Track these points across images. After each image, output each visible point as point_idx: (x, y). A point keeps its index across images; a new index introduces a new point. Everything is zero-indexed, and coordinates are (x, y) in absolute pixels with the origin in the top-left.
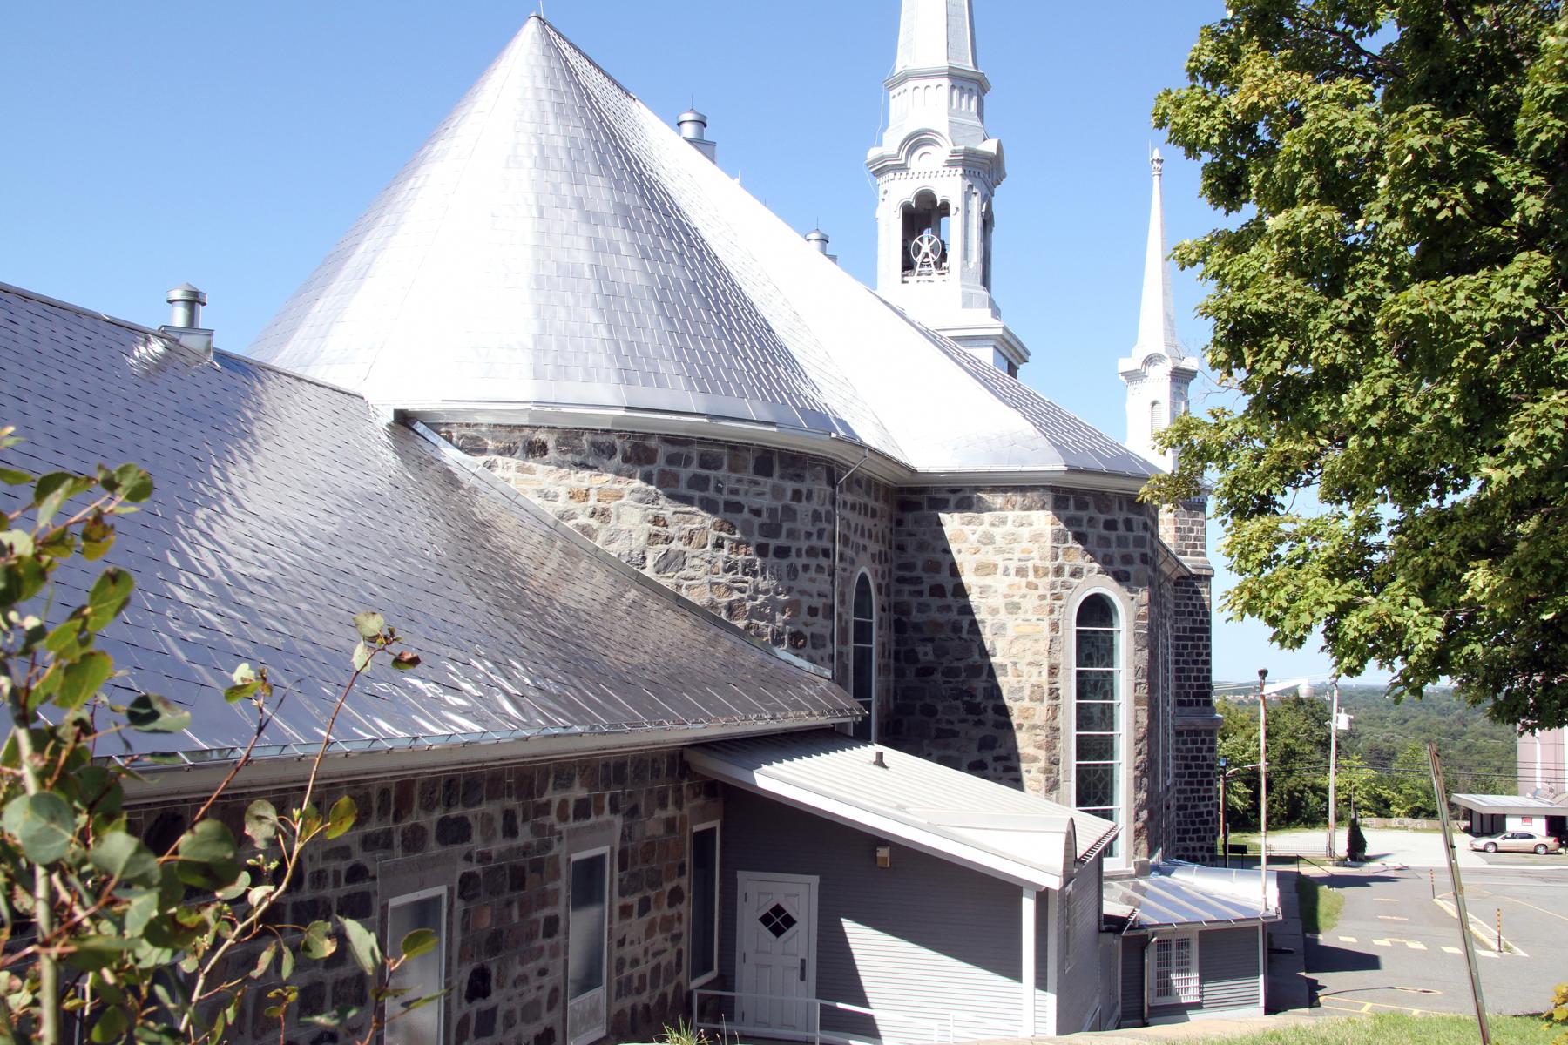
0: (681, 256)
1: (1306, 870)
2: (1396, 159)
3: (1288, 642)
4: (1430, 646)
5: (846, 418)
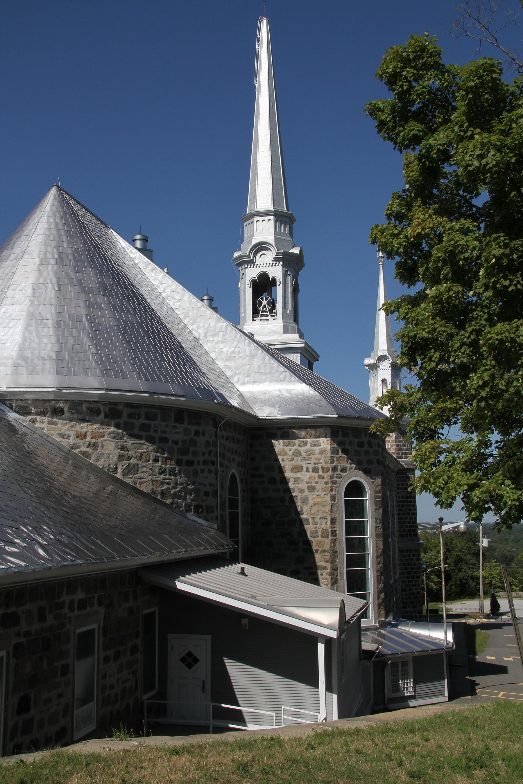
0: (134, 310)
1: (470, 621)
2: (488, 261)
3: (444, 505)
4: (514, 503)
5: (222, 392)
